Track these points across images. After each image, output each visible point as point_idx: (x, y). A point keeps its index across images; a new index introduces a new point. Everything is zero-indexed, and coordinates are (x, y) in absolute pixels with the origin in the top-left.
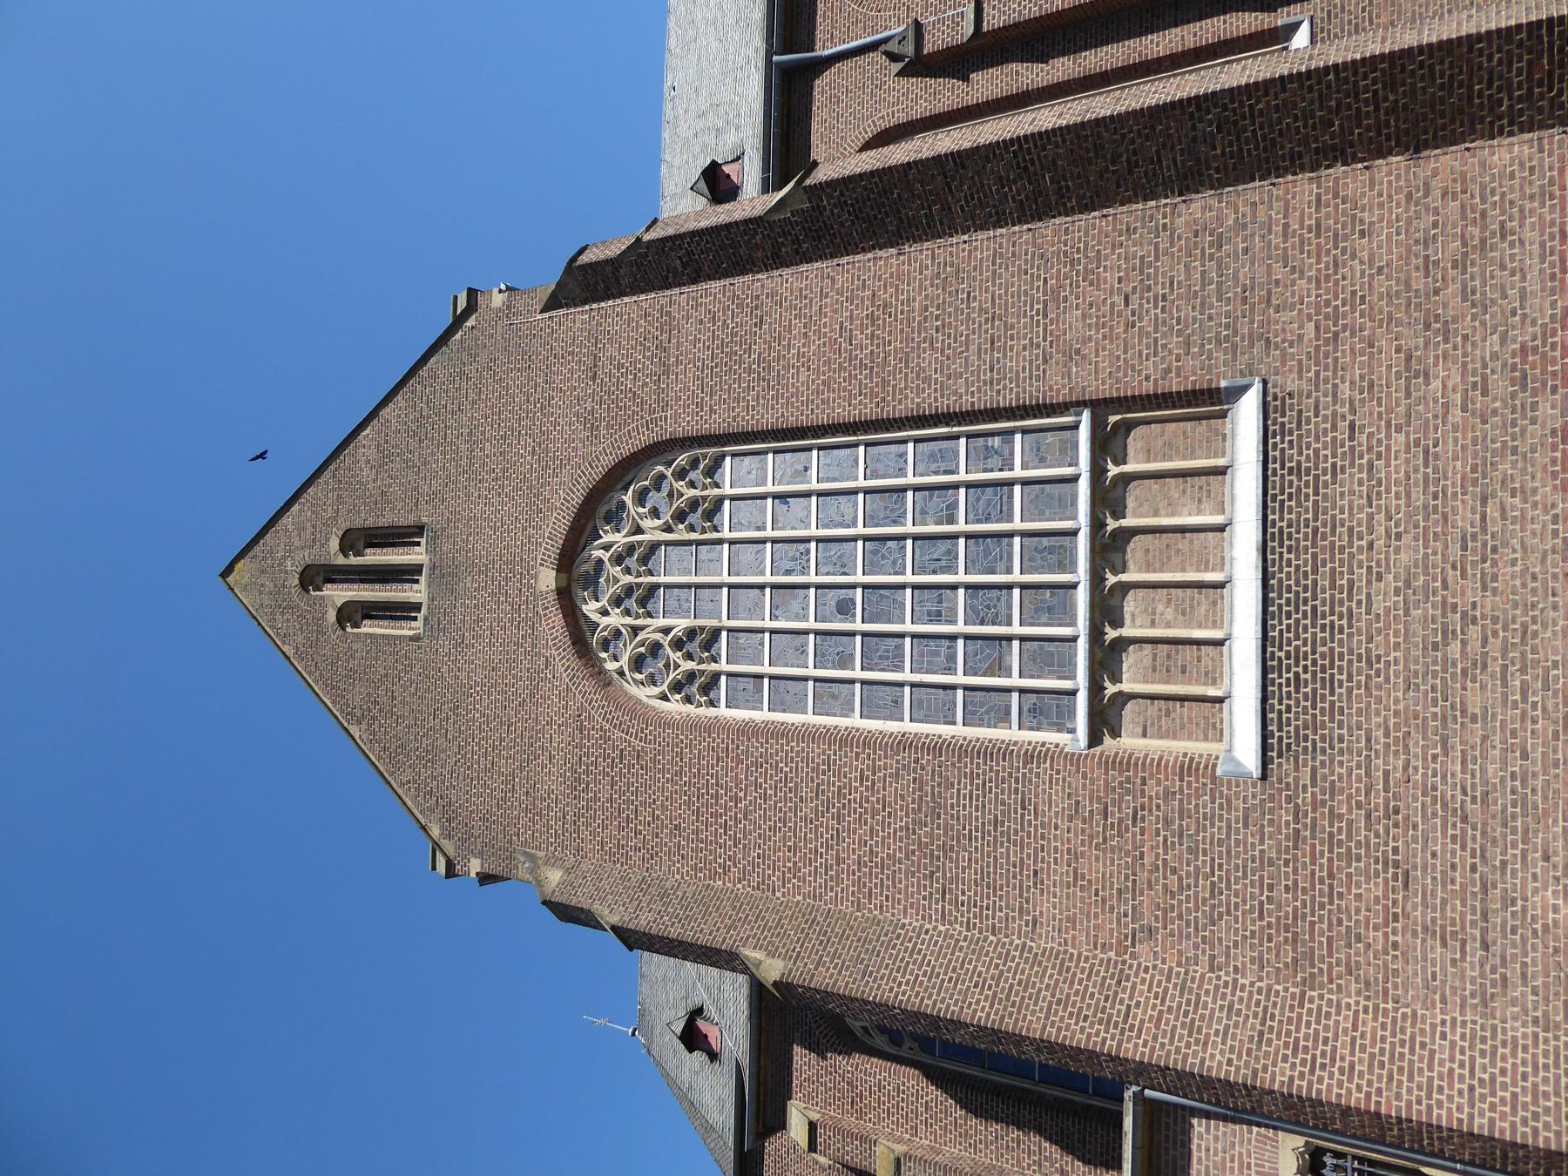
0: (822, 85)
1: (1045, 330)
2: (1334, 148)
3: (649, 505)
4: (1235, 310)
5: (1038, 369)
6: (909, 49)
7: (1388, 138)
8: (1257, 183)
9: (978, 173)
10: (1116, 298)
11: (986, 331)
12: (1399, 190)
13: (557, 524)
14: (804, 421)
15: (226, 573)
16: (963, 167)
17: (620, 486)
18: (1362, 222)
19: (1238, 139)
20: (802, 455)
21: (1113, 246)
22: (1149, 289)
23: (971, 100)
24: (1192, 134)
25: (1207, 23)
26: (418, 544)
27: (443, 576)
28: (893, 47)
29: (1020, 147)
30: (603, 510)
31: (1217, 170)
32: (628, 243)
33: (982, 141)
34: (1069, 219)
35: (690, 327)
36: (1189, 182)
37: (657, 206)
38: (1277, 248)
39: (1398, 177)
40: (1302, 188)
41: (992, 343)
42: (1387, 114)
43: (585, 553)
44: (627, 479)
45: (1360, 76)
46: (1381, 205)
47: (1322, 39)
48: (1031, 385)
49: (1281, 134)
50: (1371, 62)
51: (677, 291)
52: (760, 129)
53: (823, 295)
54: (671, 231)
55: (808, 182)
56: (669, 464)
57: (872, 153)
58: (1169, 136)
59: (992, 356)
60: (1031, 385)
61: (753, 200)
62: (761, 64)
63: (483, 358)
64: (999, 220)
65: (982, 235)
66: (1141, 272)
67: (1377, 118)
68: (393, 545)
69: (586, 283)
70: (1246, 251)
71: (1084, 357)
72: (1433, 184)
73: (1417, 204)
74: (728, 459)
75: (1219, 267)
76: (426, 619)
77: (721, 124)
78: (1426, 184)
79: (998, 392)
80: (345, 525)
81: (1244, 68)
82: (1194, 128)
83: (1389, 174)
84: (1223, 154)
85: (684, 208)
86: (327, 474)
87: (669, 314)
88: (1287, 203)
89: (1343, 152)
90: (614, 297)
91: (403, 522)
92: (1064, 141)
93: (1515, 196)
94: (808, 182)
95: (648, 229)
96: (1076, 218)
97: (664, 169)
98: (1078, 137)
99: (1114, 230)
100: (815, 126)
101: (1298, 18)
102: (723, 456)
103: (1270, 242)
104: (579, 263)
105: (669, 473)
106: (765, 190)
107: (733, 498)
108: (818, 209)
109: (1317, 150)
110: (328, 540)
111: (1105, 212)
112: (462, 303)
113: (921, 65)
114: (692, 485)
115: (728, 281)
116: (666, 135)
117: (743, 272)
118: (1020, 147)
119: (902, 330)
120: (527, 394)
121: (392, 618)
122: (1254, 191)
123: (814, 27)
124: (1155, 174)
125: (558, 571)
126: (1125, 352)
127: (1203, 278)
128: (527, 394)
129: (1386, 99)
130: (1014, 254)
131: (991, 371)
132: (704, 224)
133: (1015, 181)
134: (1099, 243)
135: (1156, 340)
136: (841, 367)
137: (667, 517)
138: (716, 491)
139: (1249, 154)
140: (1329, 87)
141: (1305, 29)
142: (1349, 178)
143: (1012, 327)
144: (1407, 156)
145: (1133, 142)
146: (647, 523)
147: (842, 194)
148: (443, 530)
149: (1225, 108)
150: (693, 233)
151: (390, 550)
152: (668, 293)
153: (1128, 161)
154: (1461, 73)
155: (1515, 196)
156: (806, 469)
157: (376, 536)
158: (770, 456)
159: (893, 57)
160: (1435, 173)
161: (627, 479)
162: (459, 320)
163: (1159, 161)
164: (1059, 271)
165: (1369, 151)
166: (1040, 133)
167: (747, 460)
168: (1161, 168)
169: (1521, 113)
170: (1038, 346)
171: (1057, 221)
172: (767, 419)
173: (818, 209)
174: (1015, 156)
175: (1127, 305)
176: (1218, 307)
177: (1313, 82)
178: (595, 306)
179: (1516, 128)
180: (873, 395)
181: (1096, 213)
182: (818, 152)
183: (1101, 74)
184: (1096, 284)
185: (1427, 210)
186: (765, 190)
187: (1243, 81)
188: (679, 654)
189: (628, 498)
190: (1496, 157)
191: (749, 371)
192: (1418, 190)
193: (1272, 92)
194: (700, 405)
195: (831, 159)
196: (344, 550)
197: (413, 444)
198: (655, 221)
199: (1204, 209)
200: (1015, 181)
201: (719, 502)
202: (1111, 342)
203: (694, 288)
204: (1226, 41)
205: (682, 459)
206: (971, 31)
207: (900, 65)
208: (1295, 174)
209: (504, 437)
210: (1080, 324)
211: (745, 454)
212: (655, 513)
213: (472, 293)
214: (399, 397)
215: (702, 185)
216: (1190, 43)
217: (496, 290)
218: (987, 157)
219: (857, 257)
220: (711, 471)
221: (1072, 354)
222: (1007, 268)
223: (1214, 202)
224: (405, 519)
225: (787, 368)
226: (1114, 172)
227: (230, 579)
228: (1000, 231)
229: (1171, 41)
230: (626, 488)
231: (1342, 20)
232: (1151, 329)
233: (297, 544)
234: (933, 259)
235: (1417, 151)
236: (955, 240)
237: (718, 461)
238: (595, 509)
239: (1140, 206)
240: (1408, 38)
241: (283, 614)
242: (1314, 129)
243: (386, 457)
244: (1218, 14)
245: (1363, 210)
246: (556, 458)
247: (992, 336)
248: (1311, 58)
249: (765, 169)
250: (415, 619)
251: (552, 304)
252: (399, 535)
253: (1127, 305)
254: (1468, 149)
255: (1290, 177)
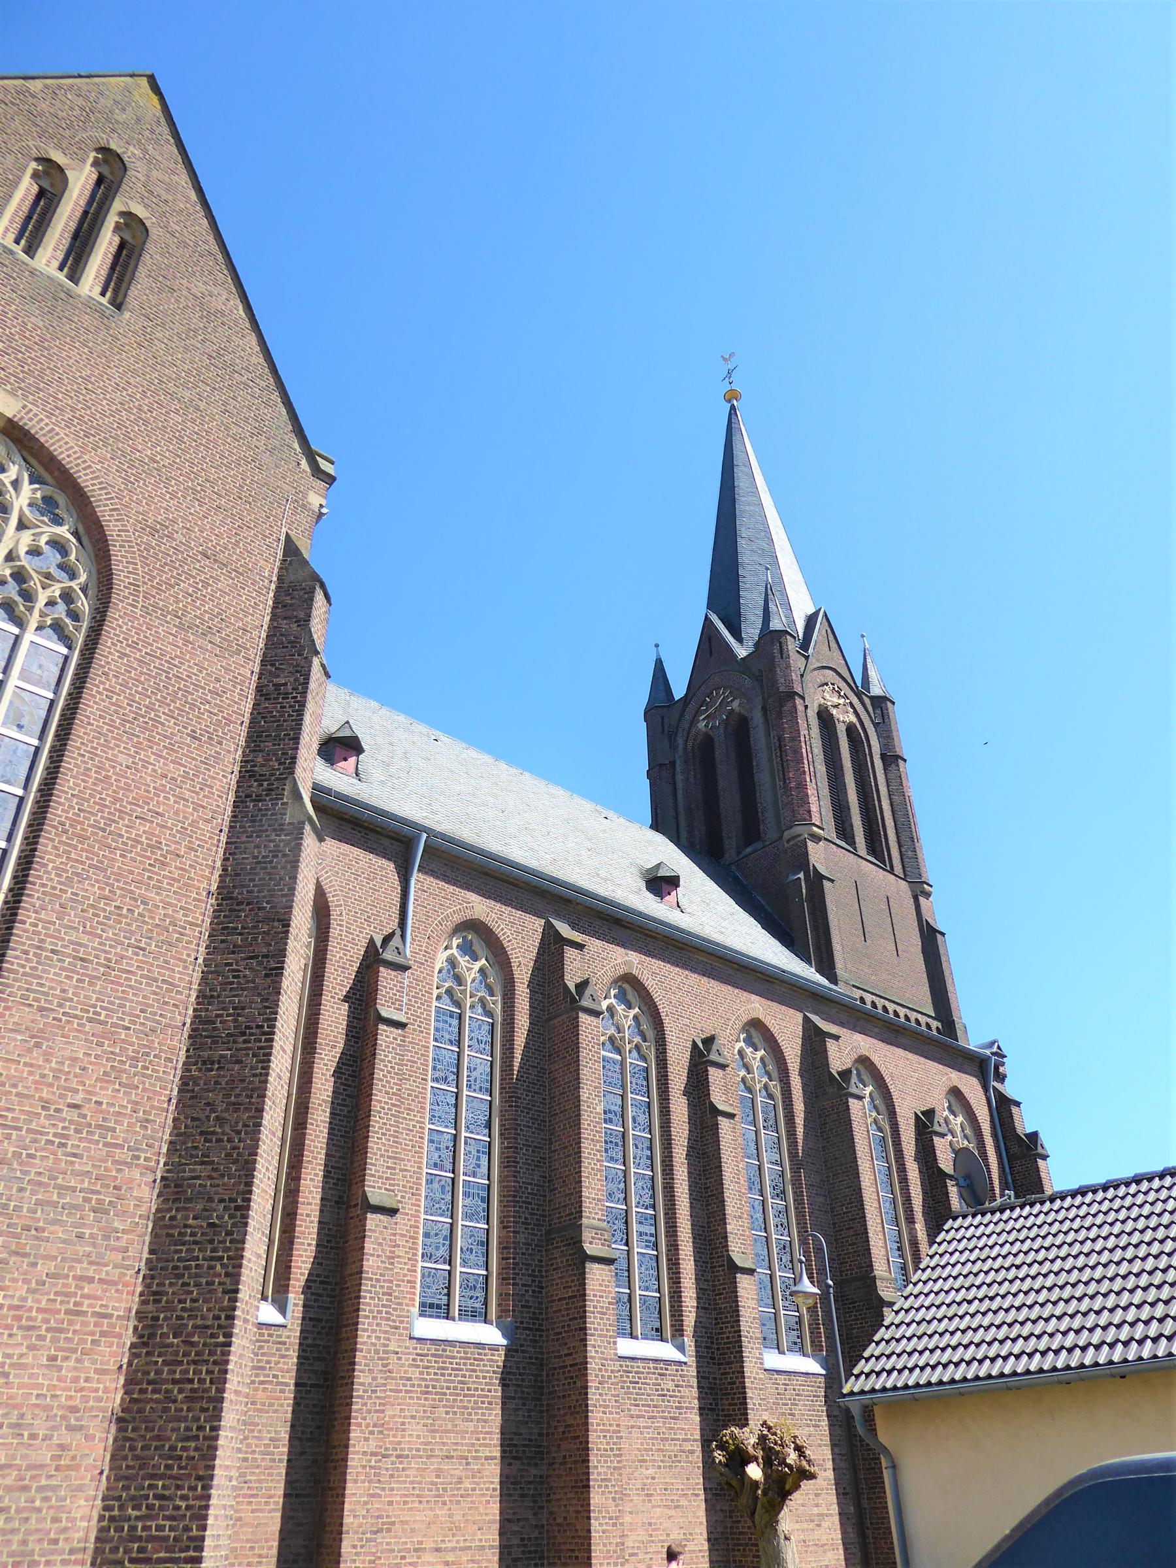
0: (387, 869)
1: (76, 1017)
2: (152, 1336)
3: (46, 549)
4: (19, 1217)
5: (35, 1000)
6: (389, 955)
7: (142, 1391)
8: (145, 1255)
9: (256, 988)
10: (81, 1095)
11: (97, 957)
12: (85, 1399)
13: (63, 444)
14: (74, 743)
15: (152, 79)
16: (267, 975)
17: (81, 530)
18: (66, 1359)
19: (196, 1243)
20: (37, 729)
21: (137, 1103)
22: (77, 1131)
23: (326, 998)
24: (216, 1198)
25: (314, 1229)
26: (103, 294)
27: (56, 302)
28: (396, 941)
29: (264, 1034)
30: (61, 499)
31: (172, 1218)
32: (317, 642)
33: (283, 998)
34: (180, 1065)
35: (216, 667)
36: (173, 1189)
37: (341, 684)
38: (71, 1268)
39: (99, 1399)
40: (124, 1301)
41: (82, 960)
42: (167, 1391)
43: (18, 458)
44: (85, 540)
45: (211, 1367)
46: (76, 1380)
47: (262, 1335)
48: (20, 988)
49: (185, 1284)
50: (220, 1380)
51: (257, 669)
52: (374, 802)
53: (197, 806)
54: (313, 685)
55: (308, 828)
56: (84, 590)
57: (311, 895)
58: (222, 1176)
59: (69, 956)
60: (20, 988)
61: (311, 771)
62: (427, 823)
63: (266, 458)
64: (204, 997)
65: (197, 976)
66: (99, 1127)
67: (165, 1381)
68: (113, 268)
69: (296, 589)
70: (80, 1236)
71: (29, 1050)
72: (79, 1435)
73: (63, 1417)
74: (65, 651)
75: (74, 1207)
76: (12, 252)
77: (392, 770)
78: (81, 1428)
79: (26, 953)
80: (154, 232)
81: (259, 1256)
82: (222, 1201)
83: (106, 1390)
84: (186, 1226)
85: (329, 707)
86: (215, 248)
87: (238, 653)
88: (115, 1283)
89: (145, 1344)
90: (274, 608)
91: (134, 292)
92: (255, 1075)
93: (33, 1524)
94: (308, 828)
95: (323, 666)
96: (179, 1072)
97: (374, 704)
98: (253, 1090)
99: (152, 1107)
100: (356, 851)
101: (289, 1314)
102: (70, 648)
103: (80, 1261)
104: (318, 589)
105: (74, 584)
106: (316, 787)
107: (17, 639)
108: (280, 830)
109: (156, 1319)
110: (146, 206)
111: (174, 1101)
112: (324, 465)
113: (372, 961)
114: (51, 603)
115: (247, 721)
116: (402, 718)
117: (249, 738)
118: (264, 1034)
119: (131, 872)
120: (213, 483)
121: (29, 218)
122: (139, 1251)
123: (437, 878)
124: (192, 1156)
125: (10, 420)
126: (18, 1095)
127: (68, 1188)
128: (213, 483)
129: (180, 1391)
130: (166, 1003)
131: (53, 951)
132: (307, 718)
133: (235, 1021)
134: (144, 1090)
135: (19, 1129)
136: (117, 800)
137: (25, 561)
138: (33, 625)
139: (177, 1252)
140: (213, 1336)
141: (277, 1318)
142: (116, 1350)
143: (91, 984)
144: (118, 1409)
145: (229, 1140)
146: (26, 538)
147: (285, 855)
148: (108, 328)
149: (228, 1234)
150: (303, 705)
151: (109, 261)
152: (258, 660)
153: (214, 1133)
154: (180, 1468)
155: (33, 1524)
156: (20, 727)
157: (129, 256)
158: (51, 696)
159: (387, 939)
160: (89, 1438)
161: (85, 540)
162: (311, 456)
163: (203, 1163)
164: (132, 1044)
165: (136, 1371)
166: (270, 1054)
167: (56, 671)
168: (196, 1163)
169: (120, 1529)
170: (60, 1006)
171: (183, 1052)
172: (90, 707)
173: (280, 830)
174: (258, 1027)
175: (69, 1106)
176: (30, 1198)
177: (223, 1321)
178: (273, 586)
179: (105, 1523)
180: (74, 822)
181: (175, 1093)
182: (332, 846)
183: (305, 1123)
184: (105, 1079)
185: (54, 1428)
186: (316, 787)
187: (247, 1254)
188: (57, 594)
189: (64, 531)
190: (82, 1502)
191: (150, 708)
192: (77, 1419)
193: (228, 1280)
194: (134, 646)
195: (321, 855)
196: (127, 215)
197: (211, 348)
198: (327, 675)
199: (140, 1199)
200: (235, 1021)
201: (20, 623)
202: (35, 1082)
203: (253, 686)
204: (292, 1243)
205: (84, 605)
206: (384, 1014)
207: (379, 944)
208: (141, 1295)
209: (180, 440)
210: (67, 1054)
211: (62, 670)
212: (35, 552)
213: (330, 480)
214: (262, 360)
215: (346, 733)
216: (302, 1210)
217: (324, 502)
218: (267, 1000)
219: (221, 851)
220: (58, 628)
221: (37, 1038)
222: (155, 993)
223: (143, 1210)
224: (137, 293)
225: (139, 746)
226: (208, 1117)
227: (144, 82)
228: (194, 994)
229: (310, 1192)
230: (76, 534)
231: (274, 1355)
232: (33, 1126)
233: (155, 173)
234: (192, 924)
235: (120, 1420)
236: (202, 949)
237: (66, 639)
238: (63, 490)
239: (166, 1137)
240: (230, 1416)
241: (82, 109)
242: (179, 1318)
243: (210, 315)
244: (319, 1239)
245: (78, 1361)
246: (138, 478)
247: (91, 962)
248: (246, 1321)
249: (338, 795)
250: (17, 242)
251: (291, 549)
252: (120, 280)
253: (69, 1106)
254: (101, 1473)
255: (139, 1289)
